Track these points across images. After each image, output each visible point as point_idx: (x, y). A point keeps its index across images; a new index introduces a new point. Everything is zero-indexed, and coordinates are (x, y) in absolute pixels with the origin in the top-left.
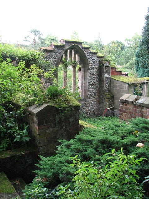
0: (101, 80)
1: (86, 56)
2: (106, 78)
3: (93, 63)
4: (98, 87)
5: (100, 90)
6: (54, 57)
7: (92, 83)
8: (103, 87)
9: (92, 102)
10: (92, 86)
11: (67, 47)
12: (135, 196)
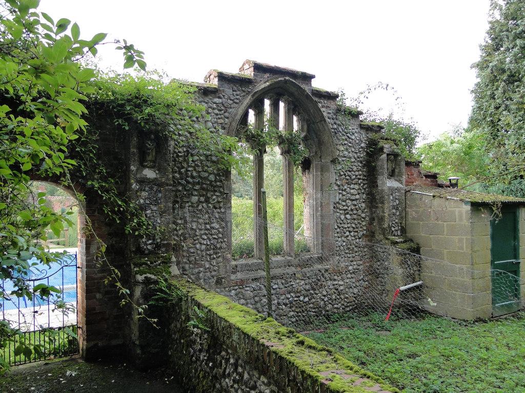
0: (373, 198)
1: (325, 121)
2: (393, 190)
3: (349, 149)
4: (367, 219)
5: (373, 231)
6: (216, 111)
7: (347, 205)
8: (381, 219)
9: (350, 268)
10: (348, 216)
11: (262, 86)
12: (249, 384)
